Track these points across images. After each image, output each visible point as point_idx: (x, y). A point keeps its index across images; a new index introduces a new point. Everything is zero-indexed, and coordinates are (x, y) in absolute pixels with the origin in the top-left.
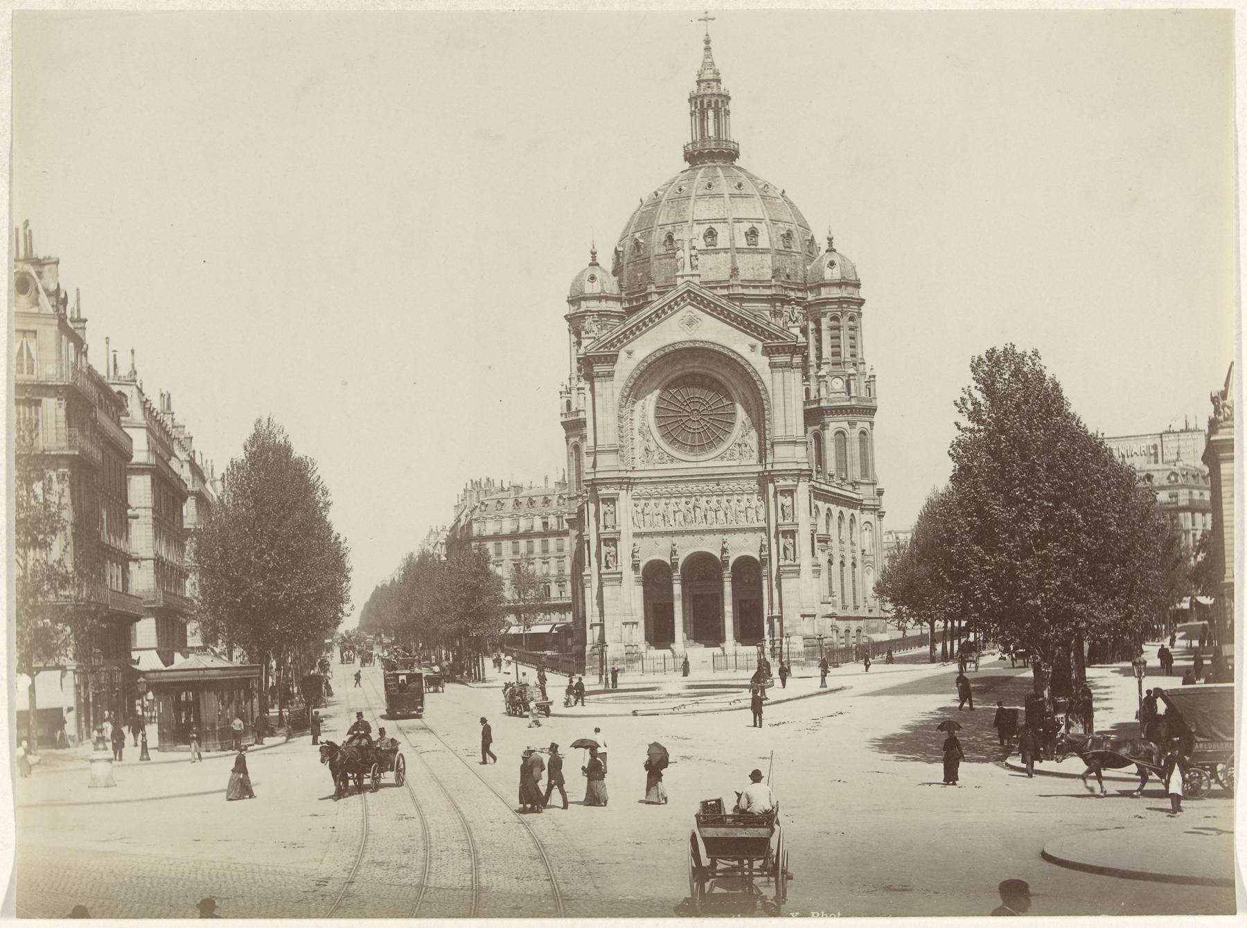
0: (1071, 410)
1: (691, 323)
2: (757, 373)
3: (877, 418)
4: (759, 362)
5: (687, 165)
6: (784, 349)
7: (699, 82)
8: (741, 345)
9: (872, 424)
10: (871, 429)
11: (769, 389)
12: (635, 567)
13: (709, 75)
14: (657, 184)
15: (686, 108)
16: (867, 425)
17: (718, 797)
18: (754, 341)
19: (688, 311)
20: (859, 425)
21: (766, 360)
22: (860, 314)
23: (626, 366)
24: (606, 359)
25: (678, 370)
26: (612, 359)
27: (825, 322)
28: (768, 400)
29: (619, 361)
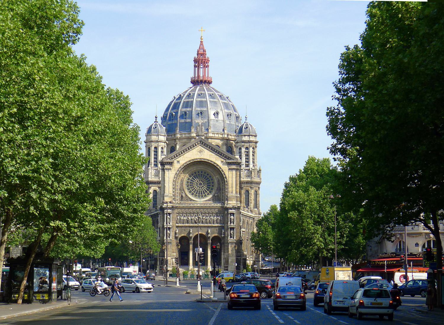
0: (328, 123)
1: (200, 152)
2: (223, 171)
3: (261, 186)
4: (225, 168)
5: (192, 85)
6: (233, 163)
7: (198, 54)
8: (218, 161)
9: (259, 188)
10: (259, 190)
11: (227, 176)
12: (176, 238)
13: (201, 51)
14: (181, 92)
15: (193, 63)
16: (257, 189)
17: (322, 272)
18: (222, 160)
19: (199, 148)
20: (254, 188)
21: (226, 166)
22: (256, 147)
23: (177, 166)
24: (169, 163)
25: (194, 169)
26: (171, 164)
27: (243, 150)
28: (226, 177)
29: (174, 164)
